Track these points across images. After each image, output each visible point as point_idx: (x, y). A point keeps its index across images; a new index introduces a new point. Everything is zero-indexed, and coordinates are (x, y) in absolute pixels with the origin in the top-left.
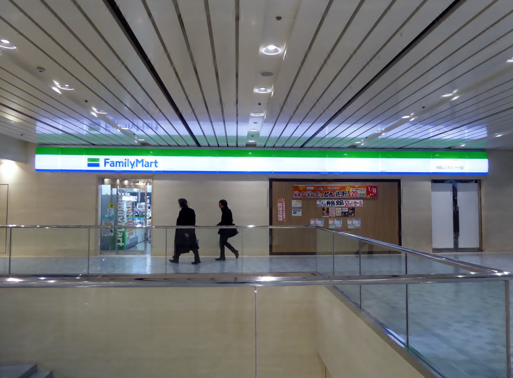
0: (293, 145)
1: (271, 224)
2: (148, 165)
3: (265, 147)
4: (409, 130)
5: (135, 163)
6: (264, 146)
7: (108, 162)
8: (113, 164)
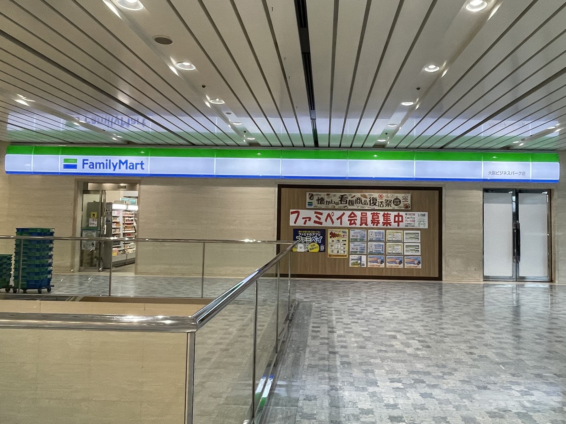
0: (397, 145)
1: (279, 238)
2: (133, 166)
3: (363, 147)
4: (516, 126)
5: (118, 164)
6: (361, 146)
7: (87, 164)
8: (92, 166)
